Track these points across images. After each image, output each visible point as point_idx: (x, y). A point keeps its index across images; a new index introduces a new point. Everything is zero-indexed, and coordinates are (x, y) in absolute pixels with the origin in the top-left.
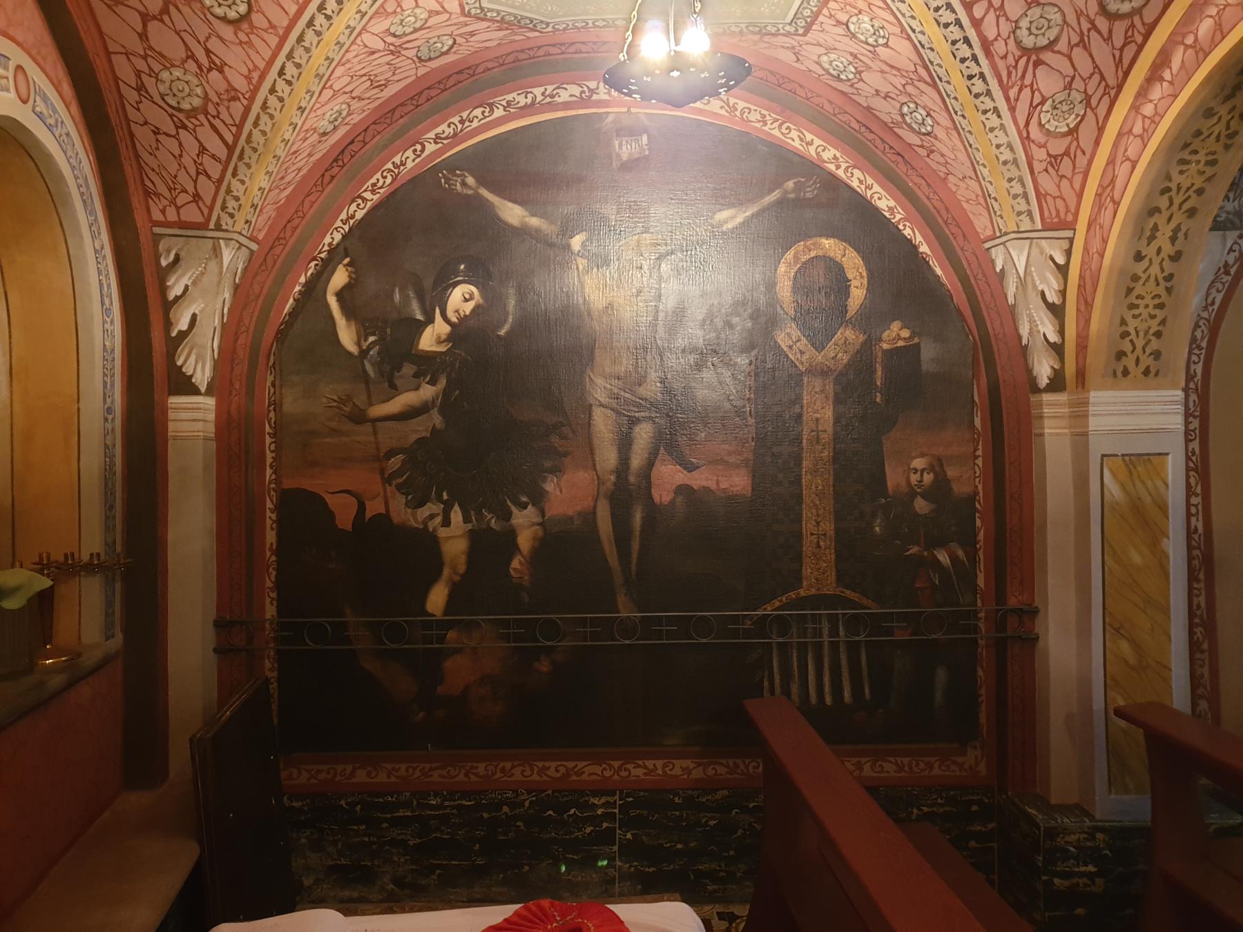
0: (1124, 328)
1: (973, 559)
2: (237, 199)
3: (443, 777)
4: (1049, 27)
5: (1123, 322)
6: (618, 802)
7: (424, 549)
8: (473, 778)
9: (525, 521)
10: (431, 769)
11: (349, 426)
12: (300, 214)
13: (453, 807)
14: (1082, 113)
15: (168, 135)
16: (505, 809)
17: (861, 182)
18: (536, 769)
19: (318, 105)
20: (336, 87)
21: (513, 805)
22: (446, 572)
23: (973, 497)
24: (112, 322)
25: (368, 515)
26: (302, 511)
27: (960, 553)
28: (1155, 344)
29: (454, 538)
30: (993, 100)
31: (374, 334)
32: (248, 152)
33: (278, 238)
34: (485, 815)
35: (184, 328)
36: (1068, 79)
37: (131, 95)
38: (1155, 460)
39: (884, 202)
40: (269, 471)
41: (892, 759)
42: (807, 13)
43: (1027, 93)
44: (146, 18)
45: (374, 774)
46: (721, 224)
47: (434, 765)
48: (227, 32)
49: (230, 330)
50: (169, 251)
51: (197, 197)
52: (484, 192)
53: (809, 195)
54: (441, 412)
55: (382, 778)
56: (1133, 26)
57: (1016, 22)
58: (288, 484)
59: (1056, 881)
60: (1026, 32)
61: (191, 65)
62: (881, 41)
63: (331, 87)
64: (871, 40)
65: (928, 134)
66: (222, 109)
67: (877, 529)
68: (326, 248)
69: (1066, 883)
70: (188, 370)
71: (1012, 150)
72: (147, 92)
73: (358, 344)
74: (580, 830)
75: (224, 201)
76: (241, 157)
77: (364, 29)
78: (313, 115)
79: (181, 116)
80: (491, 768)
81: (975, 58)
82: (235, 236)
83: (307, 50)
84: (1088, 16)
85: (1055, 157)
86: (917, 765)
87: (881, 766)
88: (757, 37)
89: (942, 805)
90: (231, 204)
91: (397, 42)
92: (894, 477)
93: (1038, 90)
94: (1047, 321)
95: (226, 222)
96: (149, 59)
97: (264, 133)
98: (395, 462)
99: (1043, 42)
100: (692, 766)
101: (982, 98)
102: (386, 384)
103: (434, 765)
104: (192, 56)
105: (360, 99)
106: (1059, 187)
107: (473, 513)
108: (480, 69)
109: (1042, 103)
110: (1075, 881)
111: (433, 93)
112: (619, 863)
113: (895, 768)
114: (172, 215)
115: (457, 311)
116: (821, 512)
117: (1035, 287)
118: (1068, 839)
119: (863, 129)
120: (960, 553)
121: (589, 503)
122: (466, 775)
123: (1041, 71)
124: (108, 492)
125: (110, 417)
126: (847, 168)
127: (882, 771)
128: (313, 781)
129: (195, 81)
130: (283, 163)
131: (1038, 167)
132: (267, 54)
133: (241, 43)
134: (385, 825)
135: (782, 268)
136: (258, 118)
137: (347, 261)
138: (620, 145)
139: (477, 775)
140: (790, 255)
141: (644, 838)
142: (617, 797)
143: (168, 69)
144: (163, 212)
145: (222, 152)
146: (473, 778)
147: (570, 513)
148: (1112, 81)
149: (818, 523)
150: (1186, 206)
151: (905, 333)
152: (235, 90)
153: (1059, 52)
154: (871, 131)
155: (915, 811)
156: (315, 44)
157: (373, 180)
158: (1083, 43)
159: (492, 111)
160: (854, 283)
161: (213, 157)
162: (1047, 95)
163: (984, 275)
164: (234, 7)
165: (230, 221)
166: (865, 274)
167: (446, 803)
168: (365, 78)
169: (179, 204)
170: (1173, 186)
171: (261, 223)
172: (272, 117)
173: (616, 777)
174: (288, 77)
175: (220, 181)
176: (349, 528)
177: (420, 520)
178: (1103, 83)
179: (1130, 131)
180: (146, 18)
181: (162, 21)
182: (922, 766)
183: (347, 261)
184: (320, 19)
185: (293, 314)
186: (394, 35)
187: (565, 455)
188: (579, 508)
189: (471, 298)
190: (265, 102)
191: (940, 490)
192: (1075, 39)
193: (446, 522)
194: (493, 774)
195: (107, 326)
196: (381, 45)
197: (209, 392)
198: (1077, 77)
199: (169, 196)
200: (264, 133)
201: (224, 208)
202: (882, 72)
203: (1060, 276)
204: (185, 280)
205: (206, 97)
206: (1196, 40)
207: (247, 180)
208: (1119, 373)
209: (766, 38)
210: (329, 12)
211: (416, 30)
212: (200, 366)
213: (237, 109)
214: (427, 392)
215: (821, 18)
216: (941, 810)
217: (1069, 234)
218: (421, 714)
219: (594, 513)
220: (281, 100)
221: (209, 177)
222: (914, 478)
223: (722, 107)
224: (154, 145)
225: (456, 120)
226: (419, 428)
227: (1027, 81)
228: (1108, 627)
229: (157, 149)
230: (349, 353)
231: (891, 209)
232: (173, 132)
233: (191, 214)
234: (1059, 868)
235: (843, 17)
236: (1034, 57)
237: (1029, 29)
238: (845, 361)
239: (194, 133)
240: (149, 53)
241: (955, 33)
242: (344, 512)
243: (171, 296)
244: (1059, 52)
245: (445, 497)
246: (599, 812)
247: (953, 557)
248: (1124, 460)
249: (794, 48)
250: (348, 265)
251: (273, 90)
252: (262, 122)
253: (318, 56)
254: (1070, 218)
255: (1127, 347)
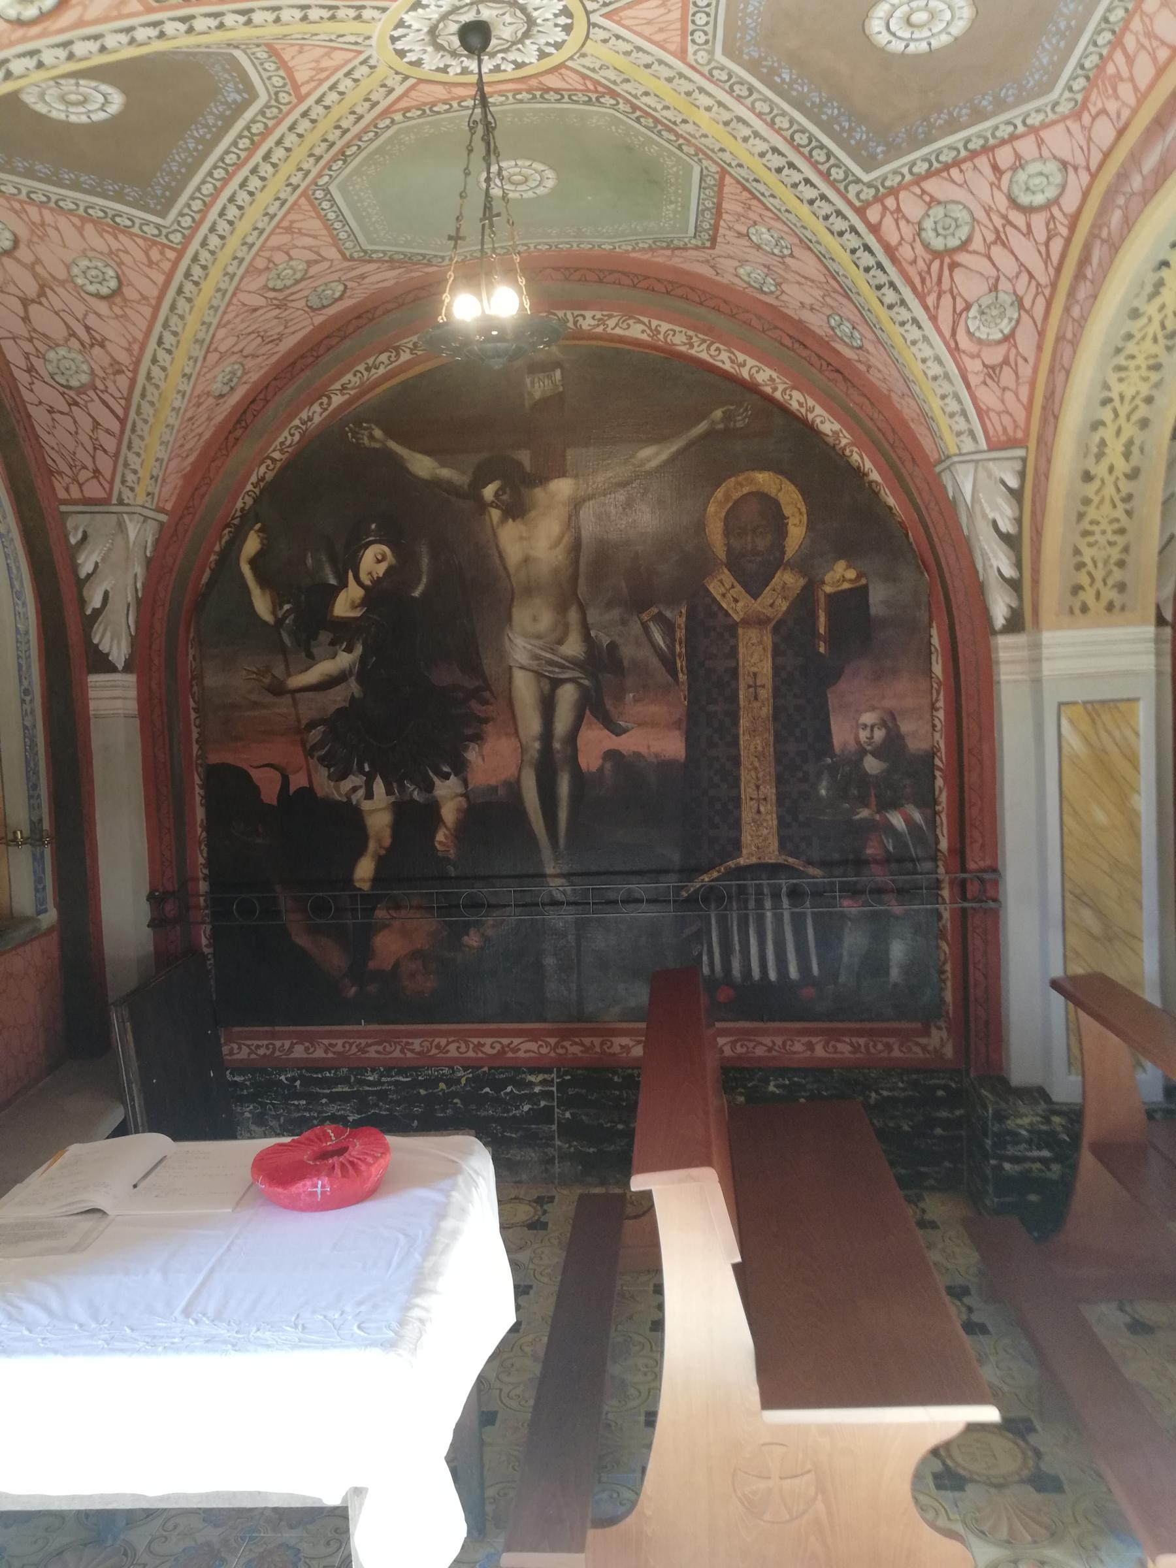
0: (1078, 559)
1: (932, 824)
2: (135, 472)
3: (377, 1052)
4: (957, 227)
5: (1077, 552)
6: (556, 1080)
7: (349, 819)
8: (409, 1055)
9: (448, 795)
10: (368, 1045)
11: (269, 699)
12: (207, 481)
13: (389, 1083)
14: (1016, 316)
15: (62, 413)
16: (442, 1085)
17: (801, 405)
18: (471, 1046)
19: (205, 370)
20: (222, 348)
21: (450, 1082)
22: (372, 846)
23: (932, 754)
24: (24, 604)
25: (292, 789)
26: (229, 788)
27: (917, 816)
28: (1117, 575)
29: (378, 814)
30: (909, 309)
31: (288, 602)
32: (140, 424)
33: (187, 508)
34: (423, 1092)
35: (98, 605)
36: (991, 281)
37: (23, 377)
38: (1123, 707)
39: (828, 426)
40: (195, 747)
41: (847, 1040)
42: (706, 226)
43: (946, 300)
44: (25, 302)
45: (311, 1050)
46: (642, 464)
47: (370, 1041)
48: (102, 307)
49: (145, 605)
50: (76, 528)
51: (97, 473)
52: (392, 445)
53: (739, 425)
54: (360, 680)
55: (319, 1053)
56: (1053, 217)
57: (919, 223)
58: (214, 758)
59: (1007, 1166)
60: (931, 234)
61: (74, 343)
62: (786, 252)
63: (216, 350)
64: (776, 251)
65: (861, 348)
66: (109, 383)
67: (823, 792)
68: (238, 514)
69: (1017, 1168)
70: (104, 647)
71: (940, 363)
72: (37, 372)
73: (274, 613)
74: (517, 1108)
75: (123, 476)
76: (133, 430)
77: (237, 288)
78: (202, 379)
79: (72, 393)
80: (426, 1044)
81: (880, 266)
82: (139, 510)
83: (182, 317)
84: (998, 211)
85: (993, 368)
86: (875, 1046)
87: (835, 1047)
88: (669, 252)
89: (904, 1090)
90: (130, 477)
91: (280, 296)
92: (842, 734)
93: (960, 295)
94: (1001, 555)
95: (127, 495)
96: (35, 341)
97: (152, 404)
98: (315, 735)
99: (954, 243)
100: (631, 1044)
101: (896, 309)
102: (303, 654)
103: (370, 1041)
104: (73, 334)
105: (254, 356)
106: (1002, 401)
107: (395, 785)
108: (379, 312)
109: (968, 307)
110: (1027, 1165)
111: (334, 341)
112: (558, 1143)
113: (850, 1048)
114: (75, 493)
115: (370, 573)
116: (761, 775)
117: (985, 515)
118: (1019, 1121)
119: (796, 345)
120: (917, 816)
121: (512, 771)
122: (402, 1051)
123: (958, 274)
124: (31, 772)
125: (28, 699)
126: (785, 390)
127: (835, 1052)
128: (253, 1056)
129: (80, 358)
130: (179, 431)
131: (974, 380)
132: (144, 325)
133: (117, 317)
134: (324, 1101)
135: (712, 509)
136: (144, 389)
137: (258, 526)
138: (533, 383)
139: (412, 1051)
140: (720, 493)
141: (584, 1118)
142: (554, 1075)
143: (51, 347)
144: (67, 490)
145: (115, 426)
146: (409, 1055)
147: (493, 782)
148: (1043, 279)
149: (758, 787)
150: (1136, 417)
151: (851, 574)
152: (118, 363)
153: (975, 252)
154: (805, 347)
155: (873, 1095)
156: (187, 310)
157: (281, 439)
158: (999, 240)
159: (398, 355)
160: (791, 521)
161: (107, 431)
162: (970, 299)
163: (937, 503)
164: (105, 283)
165: (130, 494)
166: (804, 509)
167: (383, 1079)
168: (253, 336)
169: (81, 481)
170: (1115, 395)
171: (169, 494)
172: (157, 387)
173: (552, 1054)
174: (168, 346)
175: (117, 455)
176: (275, 803)
177: (343, 793)
178: (1034, 283)
179: (1064, 337)
180: (25, 302)
181: (40, 303)
182: (880, 1047)
183: (258, 526)
184: (189, 287)
185: (211, 584)
186: (274, 290)
187: (486, 721)
188: (503, 777)
189: (384, 558)
190: (149, 373)
191: (892, 745)
192: (991, 237)
193: (369, 795)
194: (429, 1051)
195: (20, 609)
196: (262, 302)
197: (127, 669)
198: (1002, 278)
199: (69, 472)
200: (152, 404)
201: (123, 482)
202: (799, 283)
203: (1014, 502)
204: (95, 557)
205: (92, 373)
206: (1109, 233)
207: (142, 452)
208: (1078, 610)
209: (677, 252)
210: (196, 278)
211: (297, 282)
212: (115, 642)
213: (123, 381)
214: (344, 660)
215: (721, 231)
216: (903, 1095)
217: (1020, 452)
218: (354, 990)
219: (518, 781)
220: (164, 369)
221: (105, 451)
222: (863, 735)
223: (643, 332)
224: (51, 424)
225: (361, 367)
226: (338, 698)
227: (946, 284)
228: (1068, 895)
229: (54, 427)
230: (265, 623)
231: (835, 433)
232: (66, 409)
233: (94, 490)
234: (1011, 1151)
235: (743, 230)
236: (947, 260)
237: (935, 230)
238: (784, 608)
239: (85, 409)
240: (34, 335)
241: (852, 241)
242: (269, 787)
243: (83, 574)
244: (975, 252)
245: (367, 769)
246: (537, 1090)
247: (908, 821)
248: (1085, 709)
249: (708, 261)
250: (260, 531)
251: (154, 361)
252: (148, 393)
253: (193, 322)
254: (1020, 434)
255: (1084, 580)
